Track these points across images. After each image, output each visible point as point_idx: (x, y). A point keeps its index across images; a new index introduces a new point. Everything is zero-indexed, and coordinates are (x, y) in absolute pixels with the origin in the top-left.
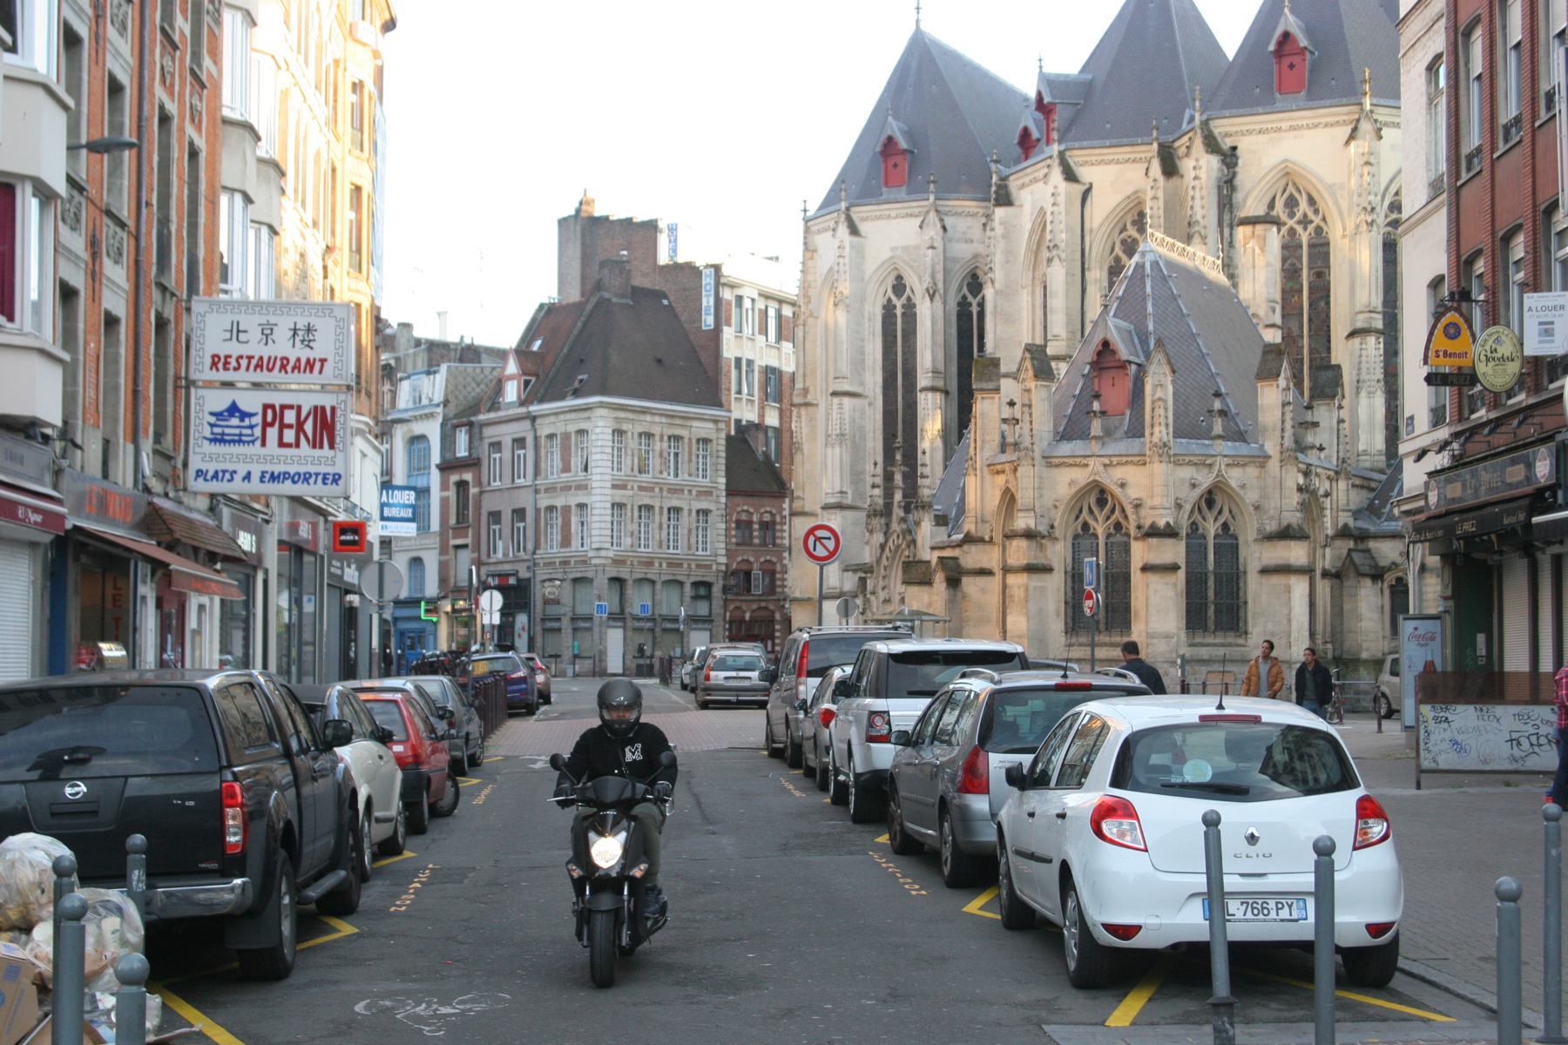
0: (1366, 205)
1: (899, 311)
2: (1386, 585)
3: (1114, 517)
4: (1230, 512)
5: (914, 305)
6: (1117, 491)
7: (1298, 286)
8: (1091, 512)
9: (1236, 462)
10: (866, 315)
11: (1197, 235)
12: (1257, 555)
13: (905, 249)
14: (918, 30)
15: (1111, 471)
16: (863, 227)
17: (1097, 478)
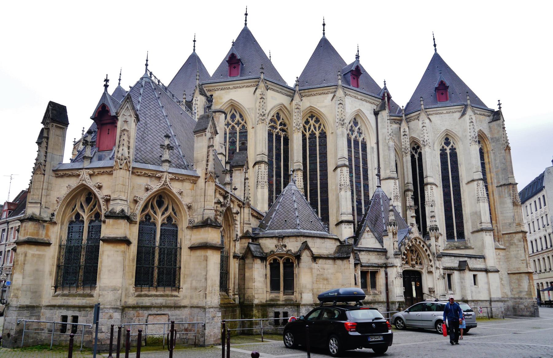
0: (261, 113)
2: (268, 263)
4: (173, 210)
6: (96, 190)
7: (235, 148)
8: (82, 207)
9: (176, 178)
12: (188, 237)
15: (93, 178)
17: (84, 183)
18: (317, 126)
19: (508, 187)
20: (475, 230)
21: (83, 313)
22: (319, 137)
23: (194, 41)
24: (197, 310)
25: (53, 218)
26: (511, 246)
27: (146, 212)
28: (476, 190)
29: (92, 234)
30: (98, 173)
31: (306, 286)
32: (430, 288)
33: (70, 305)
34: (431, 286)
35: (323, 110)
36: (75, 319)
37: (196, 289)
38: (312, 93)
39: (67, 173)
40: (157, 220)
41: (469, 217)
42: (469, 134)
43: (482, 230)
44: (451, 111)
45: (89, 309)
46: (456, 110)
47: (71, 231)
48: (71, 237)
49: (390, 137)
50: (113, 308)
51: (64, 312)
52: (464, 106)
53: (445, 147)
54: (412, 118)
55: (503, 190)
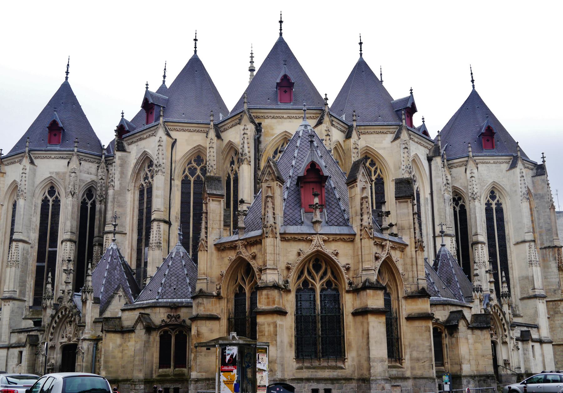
1: (51, 203)
3: (303, 278)
4: (332, 273)
5: (59, 201)
10: (34, 203)
11: (245, 160)
13: (57, 173)
14: (65, 91)
16: (36, 161)
17: (320, 249)
18: (373, 169)
19: (553, 250)
20: (525, 296)
21: (337, 385)
23: (196, 40)
24: (422, 382)
25: (288, 286)
26: (556, 315)
27: (303, 278)
28: (528, 252)
29: (325, 303)
30: (333, 240)
31: (464, 357)
32: (505, 360)
33: (319, 378)
34: (505, 357)
35: (380, 152)
37: (418, 360)
38: (369, 131)
39: (296, 237)
40: (315, 286)
41: (518, 281)
42: (520, 190)
43: (535, 297)
44: (499, 161)
45: (343, 382)
46: (504, 161)
47: (299, 299)
48: (301, 306)
49: (445, 188)
50: (384, 379)
51: (315, 386)
52: (512, 157)
53: (491, 201)
54: (454, 165)
55: (548, 253)
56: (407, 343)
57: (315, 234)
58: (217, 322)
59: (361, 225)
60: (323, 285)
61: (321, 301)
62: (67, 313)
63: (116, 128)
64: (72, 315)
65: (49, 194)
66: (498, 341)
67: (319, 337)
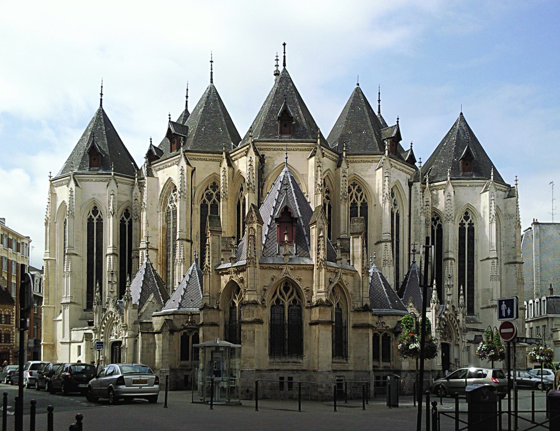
1: (95, 222)
3: (276, 297)
4: (297, 293)
5: (102, 220)
14: (101, 113)
18: (359, 195)
20: (485, 306)
21: (297, 375)
22: (361, 207)
32: (456, 359)
34: (456, 356)
36: (290, 379)
37: (359, 358)
44: (474, 184)
53: (465, 221)
56: (352, 346)
57: (285, 264)
58: (216, 328)
59: (318, 258)
60: (290, 302)
61: (288, 314)
62: (113, 316)
63: (145, 156)
64: (117, 318)
65: (93, 213)
66: (452, 344)
67: (286, 340)
